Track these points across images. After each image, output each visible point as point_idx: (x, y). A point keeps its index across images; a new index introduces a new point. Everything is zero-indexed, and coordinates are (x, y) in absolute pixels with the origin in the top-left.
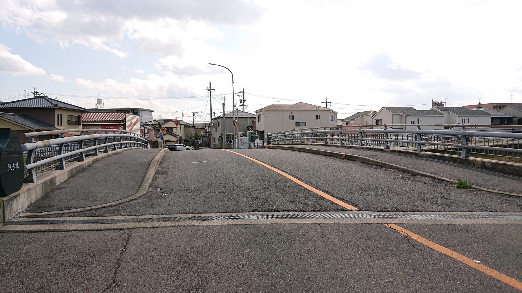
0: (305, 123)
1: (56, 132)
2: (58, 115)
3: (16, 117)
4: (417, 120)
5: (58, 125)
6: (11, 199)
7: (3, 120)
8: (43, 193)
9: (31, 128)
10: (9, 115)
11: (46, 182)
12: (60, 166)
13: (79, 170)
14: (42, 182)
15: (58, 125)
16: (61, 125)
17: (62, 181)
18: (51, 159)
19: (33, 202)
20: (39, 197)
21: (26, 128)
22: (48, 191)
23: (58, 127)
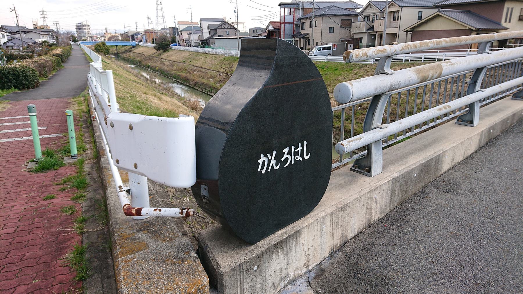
0: (422, 12)
1: (488, 37)
2: (508, 8)
3: (459, 13)
4: (309, 23)
5: (402, 61)
6: (260, 256)
7: (445, 18)
8: (392, 200)
9: (471, 26)
10: (452, 11)
11: (409, 173)
12: (468, 118)
13: (509, 125)
14: (396, 175)
15: (402, 61)
16: (510, 22)
17: (461, 159)
18: (440, 109)
19: (350, 235)
20: (376, 216)
21: (466, 27)
22: (411, 192)
23: (504, 24)
